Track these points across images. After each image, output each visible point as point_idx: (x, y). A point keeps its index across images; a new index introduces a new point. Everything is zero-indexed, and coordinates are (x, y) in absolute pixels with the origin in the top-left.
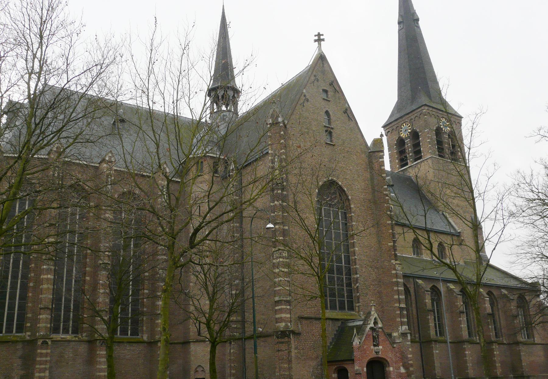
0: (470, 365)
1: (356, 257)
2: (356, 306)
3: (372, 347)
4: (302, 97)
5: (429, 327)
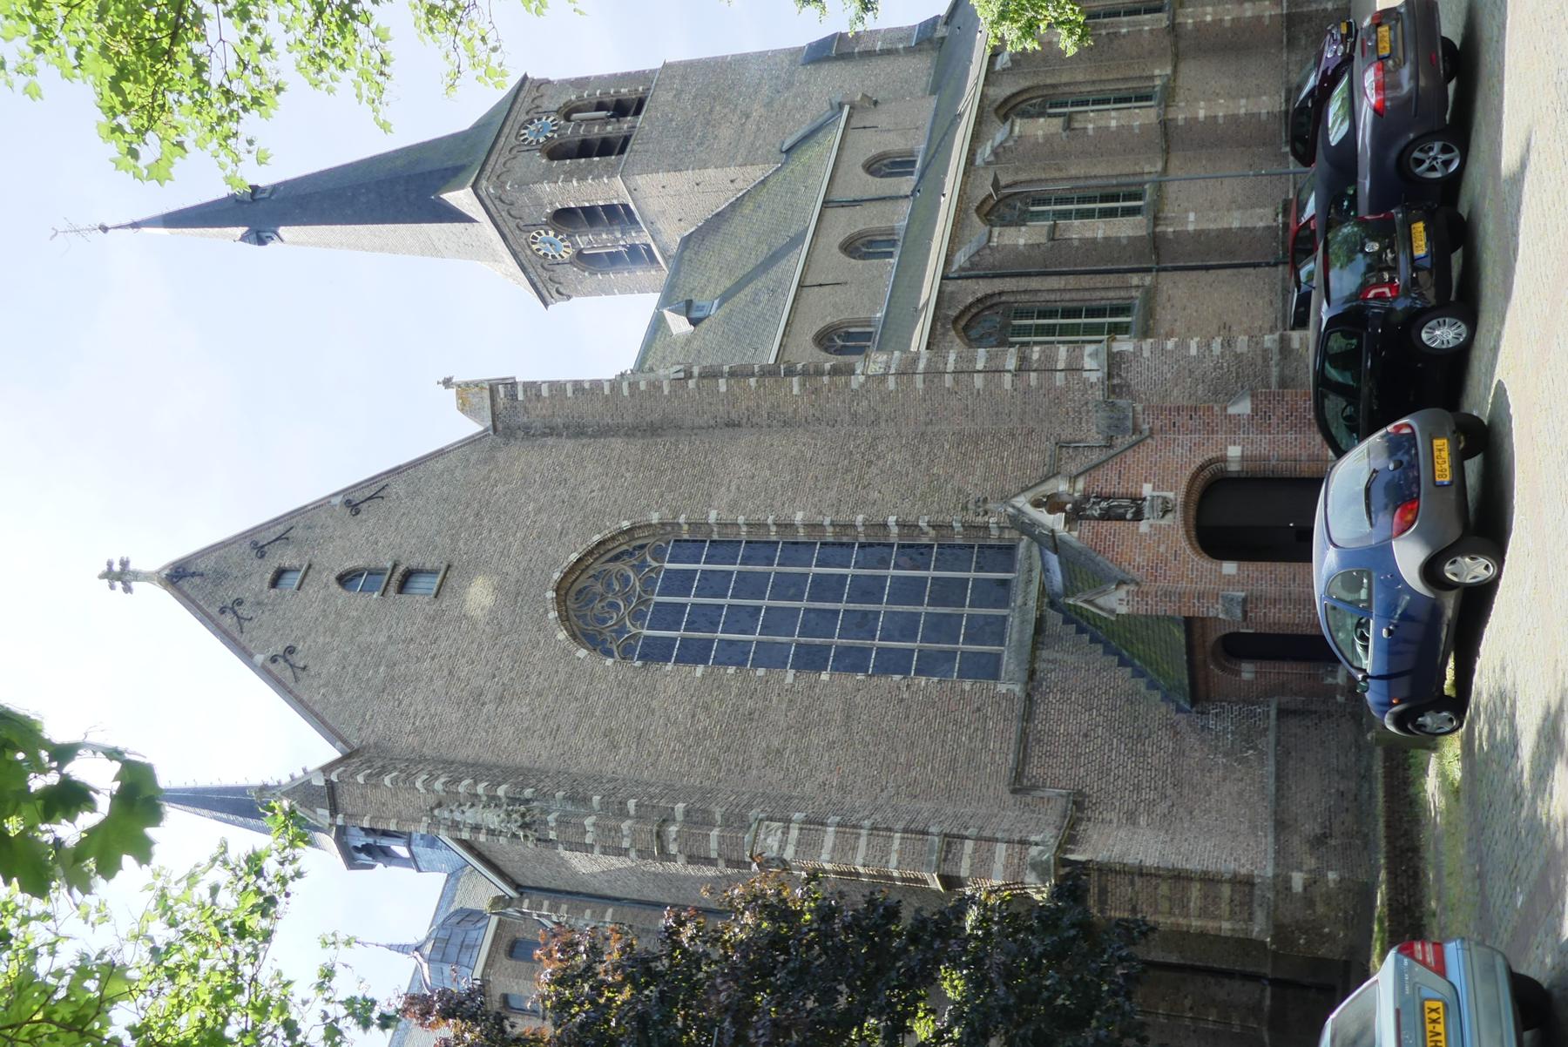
0: (1243, 107)
1: (827, 521)
3: (1144, 527)
4: (276, 672)
5: (1106, 239)
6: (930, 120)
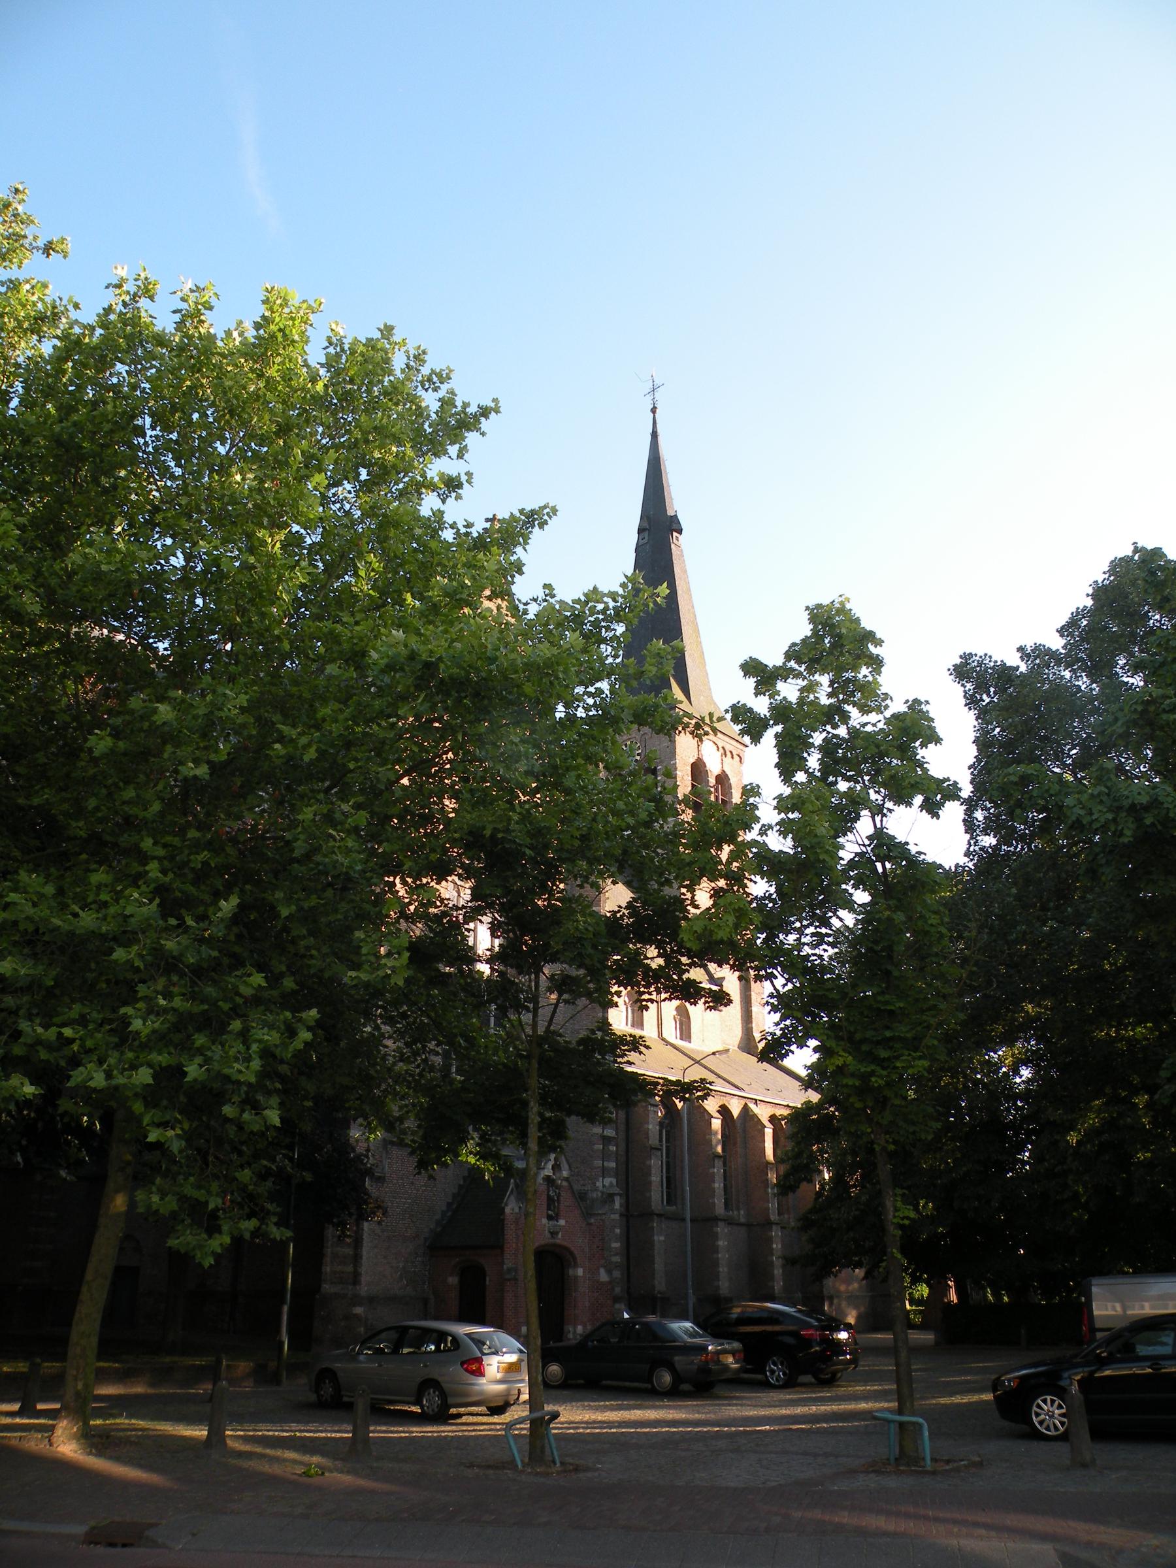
0: (723, 1269)
3: (544, 1221)
5: (650, 1183)
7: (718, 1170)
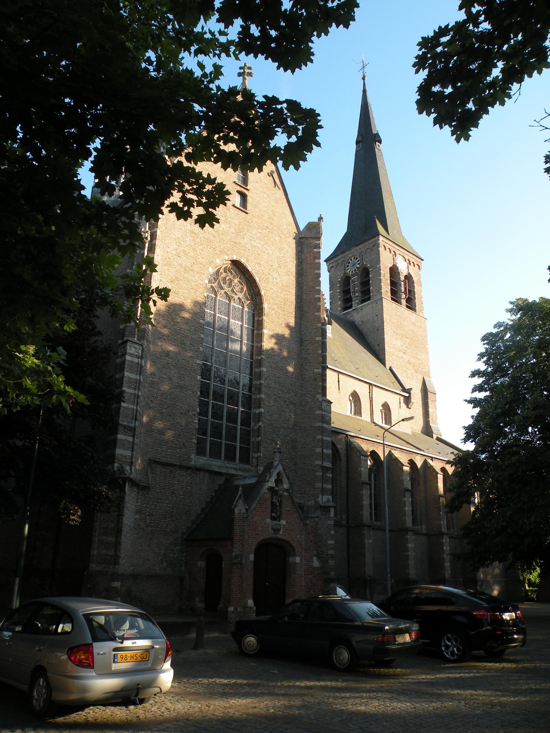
0: (411, 562)
1: (262, 382)
2: (253, 457)
3: (269, 521)
5: (362, 506)
6: (335, 427)
7: (408, 499)
